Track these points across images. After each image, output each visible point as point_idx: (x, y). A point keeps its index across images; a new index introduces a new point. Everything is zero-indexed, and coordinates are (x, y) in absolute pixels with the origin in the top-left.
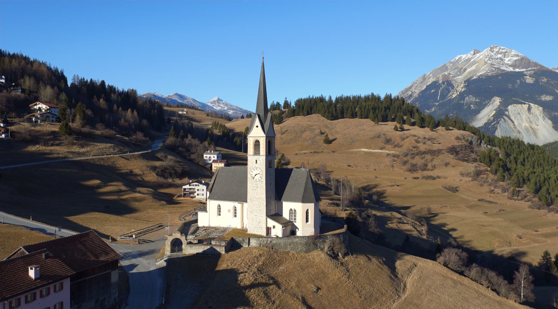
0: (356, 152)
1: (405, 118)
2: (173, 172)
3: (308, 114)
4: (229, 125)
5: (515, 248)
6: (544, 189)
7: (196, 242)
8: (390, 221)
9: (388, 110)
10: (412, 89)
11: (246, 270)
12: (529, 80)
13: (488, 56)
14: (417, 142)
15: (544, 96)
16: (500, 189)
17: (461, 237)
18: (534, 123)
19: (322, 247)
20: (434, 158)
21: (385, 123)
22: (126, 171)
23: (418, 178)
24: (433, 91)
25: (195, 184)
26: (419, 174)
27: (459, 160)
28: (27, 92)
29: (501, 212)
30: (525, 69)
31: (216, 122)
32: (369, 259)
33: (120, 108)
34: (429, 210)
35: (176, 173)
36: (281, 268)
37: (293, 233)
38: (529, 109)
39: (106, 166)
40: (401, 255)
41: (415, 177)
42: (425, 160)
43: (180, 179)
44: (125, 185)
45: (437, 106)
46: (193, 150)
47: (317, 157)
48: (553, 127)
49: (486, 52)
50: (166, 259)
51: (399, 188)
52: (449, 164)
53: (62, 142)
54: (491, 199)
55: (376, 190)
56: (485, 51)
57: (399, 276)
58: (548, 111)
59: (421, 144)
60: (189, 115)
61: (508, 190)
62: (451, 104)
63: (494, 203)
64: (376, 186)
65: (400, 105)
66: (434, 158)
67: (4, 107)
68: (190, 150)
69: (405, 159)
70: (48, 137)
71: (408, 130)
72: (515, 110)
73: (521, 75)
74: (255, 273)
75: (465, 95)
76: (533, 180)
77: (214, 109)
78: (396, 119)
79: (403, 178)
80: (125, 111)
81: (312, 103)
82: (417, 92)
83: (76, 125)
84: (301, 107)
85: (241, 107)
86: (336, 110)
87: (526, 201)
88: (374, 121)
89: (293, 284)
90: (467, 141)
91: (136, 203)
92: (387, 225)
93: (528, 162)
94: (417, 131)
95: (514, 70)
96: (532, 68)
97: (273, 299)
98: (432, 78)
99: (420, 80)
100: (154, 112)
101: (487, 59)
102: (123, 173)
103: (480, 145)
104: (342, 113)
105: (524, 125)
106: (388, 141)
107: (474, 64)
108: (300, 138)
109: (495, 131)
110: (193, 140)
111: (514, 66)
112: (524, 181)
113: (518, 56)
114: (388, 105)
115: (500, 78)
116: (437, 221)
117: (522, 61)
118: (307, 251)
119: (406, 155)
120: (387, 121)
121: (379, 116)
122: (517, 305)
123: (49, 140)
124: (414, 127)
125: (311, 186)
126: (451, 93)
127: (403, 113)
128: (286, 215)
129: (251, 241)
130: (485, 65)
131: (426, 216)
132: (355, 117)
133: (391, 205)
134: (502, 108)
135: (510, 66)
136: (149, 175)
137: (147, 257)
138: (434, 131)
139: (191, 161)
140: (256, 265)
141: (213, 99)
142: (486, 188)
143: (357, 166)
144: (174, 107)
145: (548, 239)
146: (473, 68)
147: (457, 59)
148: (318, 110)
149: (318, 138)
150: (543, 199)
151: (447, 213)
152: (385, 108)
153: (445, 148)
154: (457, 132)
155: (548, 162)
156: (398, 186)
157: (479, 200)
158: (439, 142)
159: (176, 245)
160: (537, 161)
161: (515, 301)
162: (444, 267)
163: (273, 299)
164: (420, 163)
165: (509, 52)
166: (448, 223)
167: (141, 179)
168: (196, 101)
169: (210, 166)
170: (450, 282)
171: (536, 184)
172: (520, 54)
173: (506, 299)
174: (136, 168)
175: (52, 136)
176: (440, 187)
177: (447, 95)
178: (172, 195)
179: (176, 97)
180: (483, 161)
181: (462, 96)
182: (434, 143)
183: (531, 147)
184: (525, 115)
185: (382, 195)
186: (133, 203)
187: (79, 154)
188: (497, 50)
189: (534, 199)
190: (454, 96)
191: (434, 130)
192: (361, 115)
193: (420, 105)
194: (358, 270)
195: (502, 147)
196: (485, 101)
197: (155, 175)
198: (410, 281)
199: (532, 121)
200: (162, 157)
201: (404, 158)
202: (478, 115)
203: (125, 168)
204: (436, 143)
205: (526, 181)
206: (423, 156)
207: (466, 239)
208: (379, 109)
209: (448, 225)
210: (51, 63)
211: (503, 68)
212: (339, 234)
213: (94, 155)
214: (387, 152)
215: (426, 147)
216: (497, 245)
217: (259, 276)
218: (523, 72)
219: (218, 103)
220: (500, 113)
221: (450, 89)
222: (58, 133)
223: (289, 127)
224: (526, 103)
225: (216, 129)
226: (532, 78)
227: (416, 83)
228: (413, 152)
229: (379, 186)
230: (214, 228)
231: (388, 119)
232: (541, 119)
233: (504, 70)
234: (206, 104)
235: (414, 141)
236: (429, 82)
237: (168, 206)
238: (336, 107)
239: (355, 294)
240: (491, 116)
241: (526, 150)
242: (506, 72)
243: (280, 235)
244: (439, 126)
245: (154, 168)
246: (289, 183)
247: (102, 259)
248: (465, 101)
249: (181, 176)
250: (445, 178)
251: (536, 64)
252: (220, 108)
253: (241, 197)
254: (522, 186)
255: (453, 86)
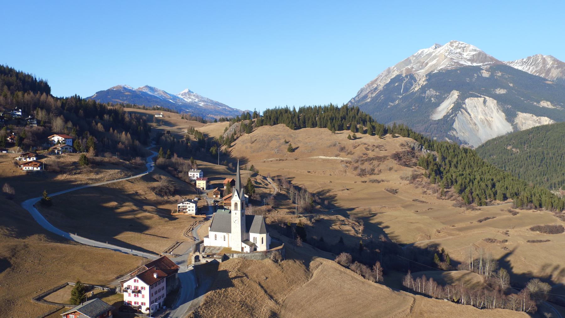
0: (315, 160)
1: (358, 126)
2: (167, 191)
3: (275, 124)
4: (203, 129)
5: (433, 240)
6: (468, 189)
7: (206, 256)
8: (334, 223)
9: (344, 120)
10: (377, 82)
11: (232, 270)
12: (486, 74)
13: (448, 50)
14: (367, 149)
15: (499, 89)
16: (431, 190)
17: (392, 233)
18: (489, 115)
19: (270, 256)
20: (380, 164)
21: (341, 132)
22: (133, 192)
23: (366, 182)
24: (397, 84)
25: (187, 202)
26: (367, 178)
27: (401, 165)
28: (42, 123)
29: (430, 210)
30: (482, 64)
31: (191, 128)
32: (295, 262)
33: (116, 131)
34: (370, 211)
35: (170, 191)
36: (249, 268)
37: (255, 249)
38: (485, 102)
39: (118, 189)
40: (314, 258)
41: (363, 181)
42: (373, 165)
43: (173, 196)
44: (135, 205)
45: (400, 99)
46: (180, 169)
47: (282, 164)
48: (506, 119)
49: (446, 46)
50: (193, 266)
51: (348, 192)
52: (392, 169)
53: (82, 170)
54: (423, 200)
55: (329, 194)
56: (445, 45)
57: (310, 270)
58: (502, 104)
59: (370, 151)
60: (165, 118)
61: (437, 191)
62: (414, 97)
63: (425, 202)
64: (329, 191)
65: (355, 114)
66: (380, 164)
67: (31, 142)
68: (177, 169)
69: (356, 165)
70: (71, 167)
71: (360, 138)
72: (472, 104)
73: (478, 69)
74: (236, 271)
75: (426, 89)
76: (459, 182)
77: (185, 101)
78: (351, 128)
79: (353, 182)
80: (120, 133)
81: (278, 114)
82: (382, 85)
83: (90, 154)
84: (268, 117)
85: (212, 99)
86: (299, 120)
87: (452, 200)
88: (331, 130)
89: (255, 276)
90: (410, 147)
91: (148, 221)
92: (331, 227)
93: (461, 164)
94: (369, 139)
95: (472, 64)
96: (488, 62)
97: (245, 283)
98: (396, 71)
99: (385, 73)
100: (141, 128)
101: (448, 53)
102: (131, 194)
103: (421, 150)
104: (304, 122)
105: (479, 117)
106: (342, 149)
107: (435, 58)
108: (267, 147)
109: (453, 124)
110: (179, 159)
111: (472, 60)
112: (453, 182)
113: (475, 50)
114: (344, 115)
115: (459, 72)
116: (374, 221)
117: (479, 56)
118: (262, 260)
119: (357, 162)
120: (343, 130)
121: (336, 126)
122: (373, 283)
123: (72, 170)
124: (366, 135)
125: (264, 225)
126: (413, 87)
127: (357, 121)
128: (251, 240)
129: (234, 255)
130: (445, 59)
131: (367, 216)
132: (315, 126)
133: (340, 207)
134: (460, 101)
135: (469, 60)
136: (150, 194)
137: (182, 264)
138: (382, 138)
139: (179, 178)
140: (237, 268)
141: (183, 92)
142: (420, 190)
143: (315, 172)
144: (150, 110)
145: (461, 233)
146: (434, 62)
147: (419, 53)
148: (283, 120)
149: (283, 146)
150: (465, 197)
151: (385, 212)
152: (341, 118)
153: (390, 155)
154: (402, 139)
155: (477, 164)
156: (348, 189)
157: (413, 200)
158: (386, 149)
159: (197, 258)
160: (468, 164)
161: (373, 281)
162: (338, 265)
163: (245, 283)
164: (369, 168)
165: (468, 47)
166: (383, 221)
167: (145, 198)
168: (166, 93)
169: (194, 182)
170: (338, 272)
171: (462, 185)
172: (478, 49)
173: (368, 280)
174: (140, 190)
175: (74, 167)
176: (383, 190)
177: (410, 87)
178: (169, 211)
179: (147, 90)
180: (422, 165)
181: (423, 89)
182: (381, 150)
183: (464, 150)
184: (480, 108)
185: (334, 198)
186: (146, 221)
187: (97, 180)
188: (456, 45)
189: (458, 199)
190: (416, 89)
191: (382, 137)
192: (321, 125)
193: (385, 98)
194: (288, 268)
195: (439, 151)
196: (444, 94)
197: (154, 194)
198: (315, 273)
199: (487, 113)
200: (157, 178)
201: (355, 164)
202: (438, 108)
203: (132, 190)
204: (383, 149)
205: (454, 183)
206: (371, 162)
207: (396, 234)
208: (336, 119)
209: (383, 223)
210: (36, 75)
211: (462, 62)
212: (278, 250)
213: (107, 180)
214: (341, 158)
215: (374, 154)
216: (419, 239)
217: (239, 273)
218: (480, 66)
219: (189, 95)
220: (458, 107)
221: (412, 82)
222: (78, 163)
223: (257, 136)
224: (482, 96)
225: (192, 134)
226: (488, 72)
227: (381, 76)
228: (363, 159)
229: (332, 191)
230: (213, 247)
231: (344, 128)
232: (495, 111)
233: (463, 65)
234: (177, 96)
235: (364, 149)
236: (393, 75)
237: (170, 222)
238: (298, 117)
239: (285, 280)
240: (450, 108)
241: (460, 154)
242: (464, 66)
243: (249, 252)
244: (387, 133)
245: (153, 189)
246: (253, 223)
247: (172, 268)
248: (426, 94)
249: (174, 194)
250: (388, 181)
251: (492, 59)
252: (190, 100)
253: (228, 230)
254: (450, 187)
255: (416, 79)
